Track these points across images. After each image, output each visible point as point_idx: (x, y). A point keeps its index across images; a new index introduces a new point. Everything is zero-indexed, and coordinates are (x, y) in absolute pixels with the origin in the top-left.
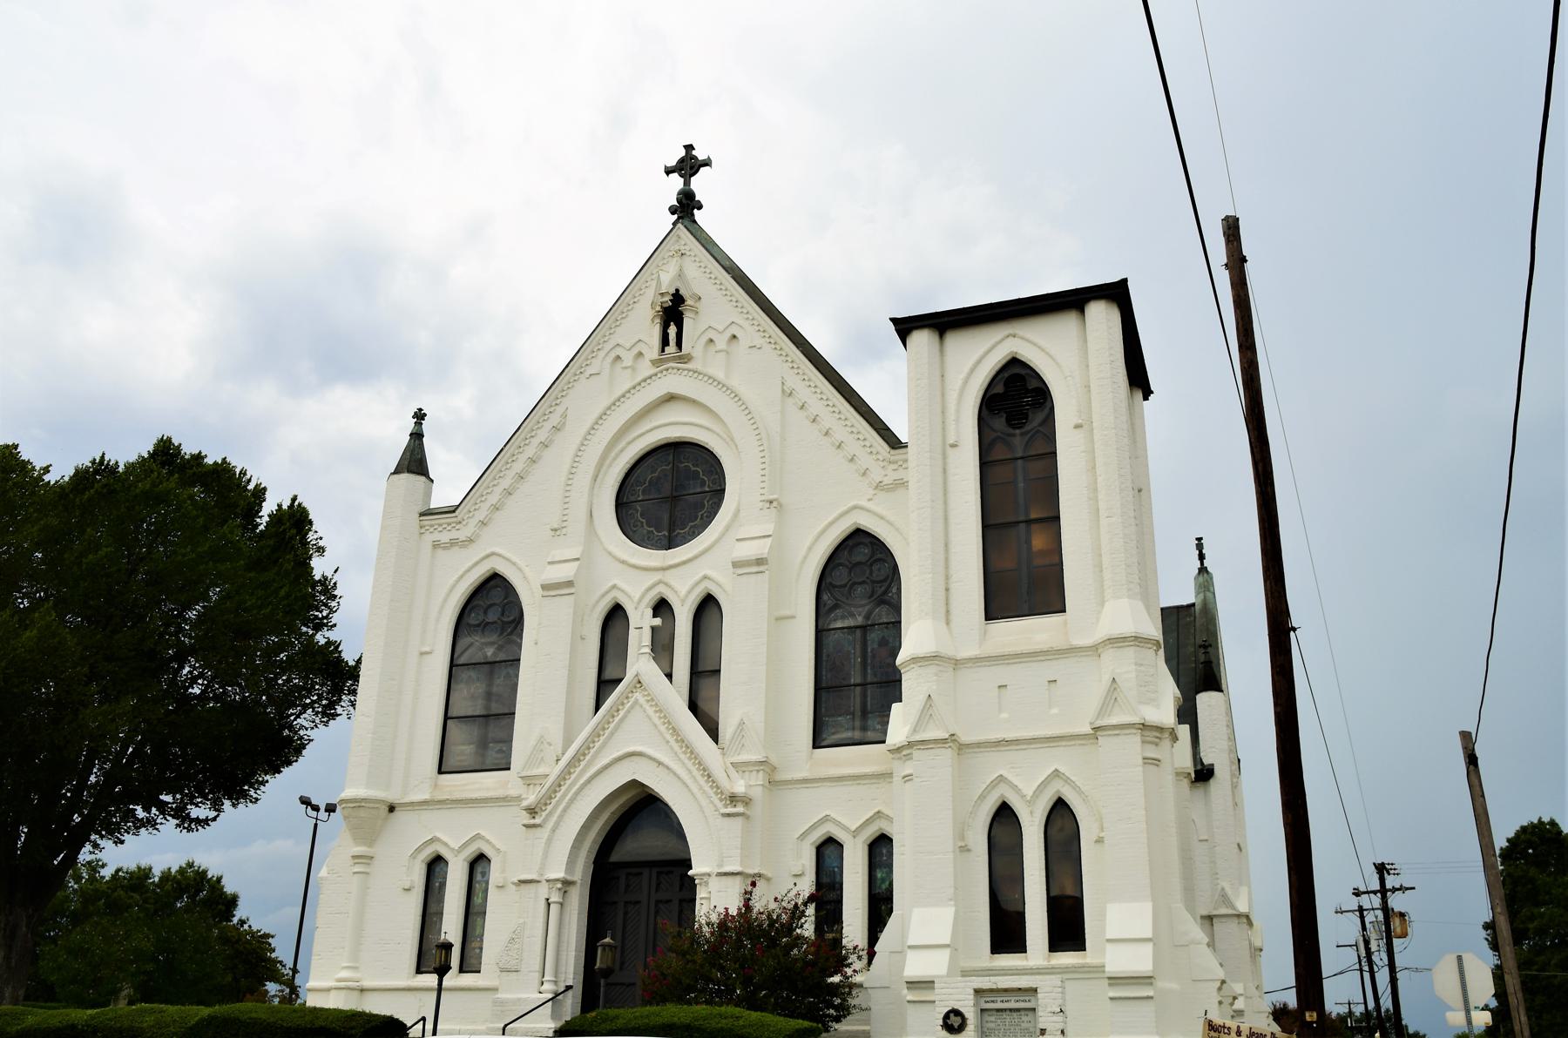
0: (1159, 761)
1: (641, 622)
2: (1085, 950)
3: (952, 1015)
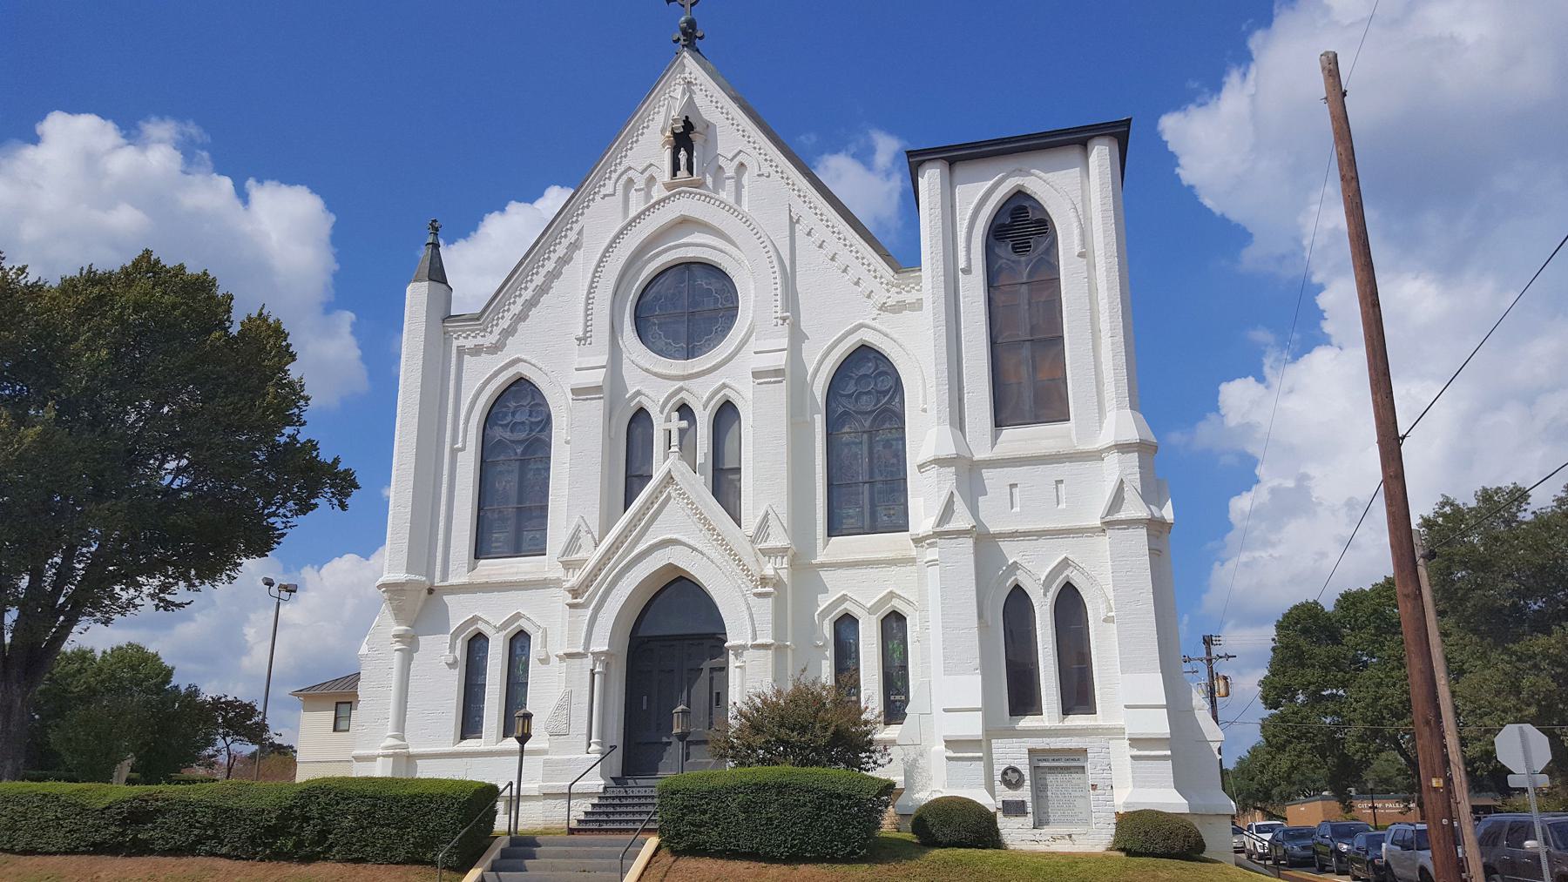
0: (1160, 552)
1: (663, 424)
2: (1095, 713)
3: (1009, 772)
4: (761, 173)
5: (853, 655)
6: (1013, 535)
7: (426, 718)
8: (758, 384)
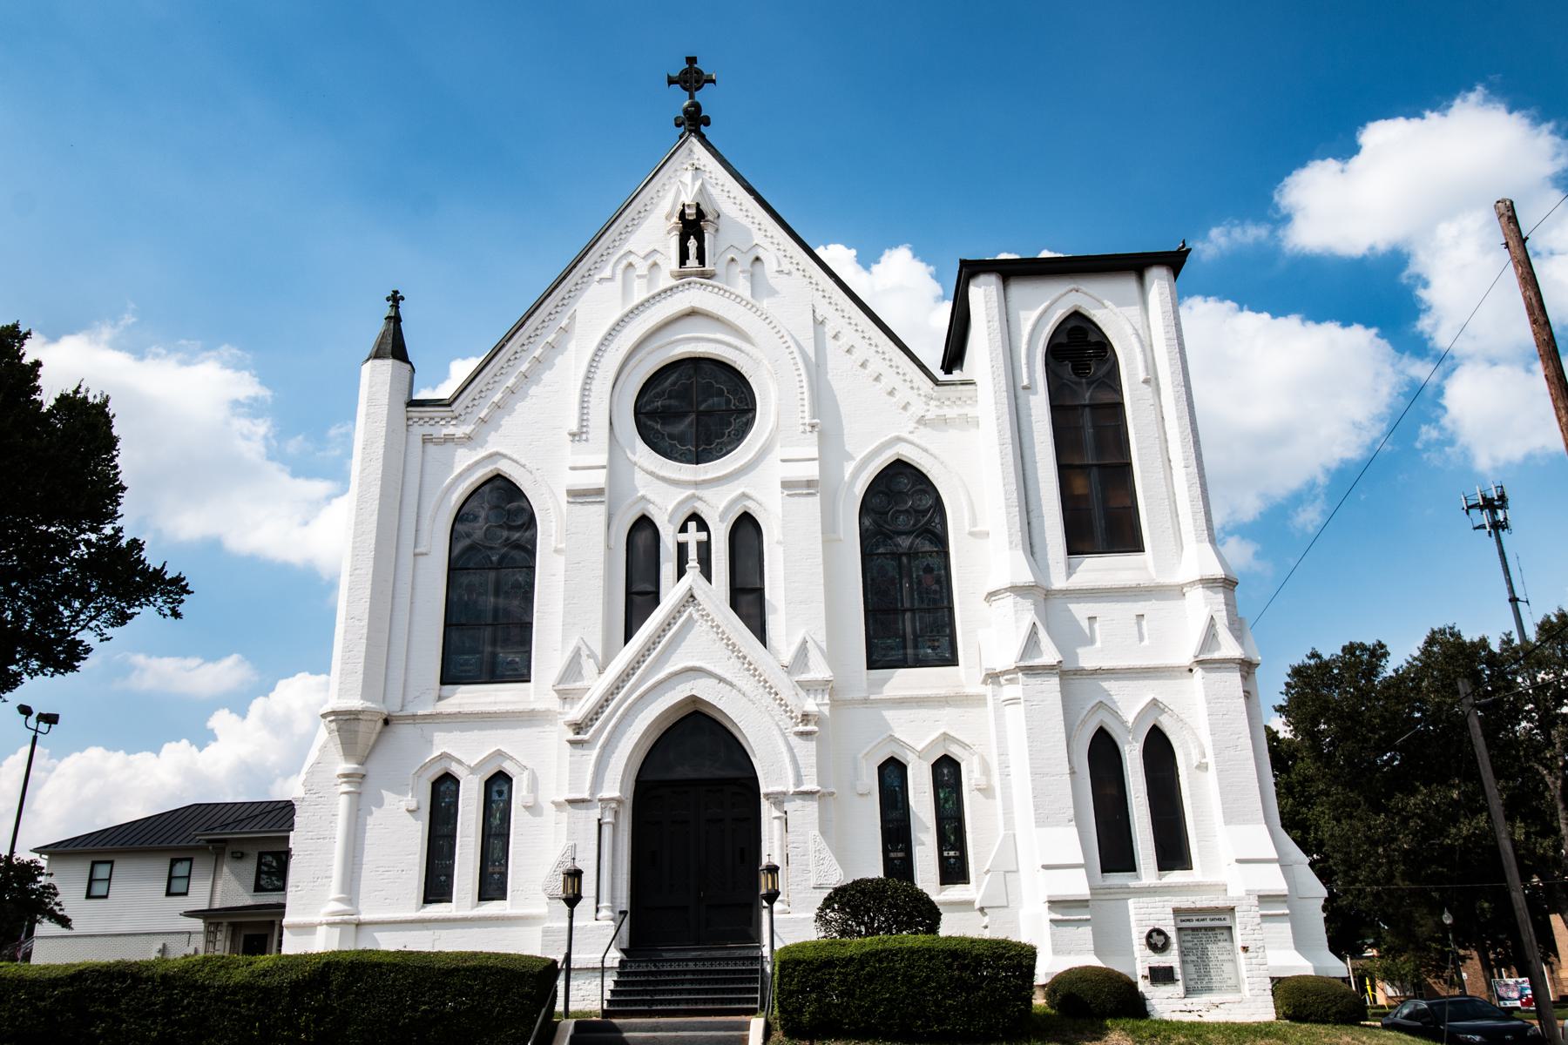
3: (1154, 934)
4: (780, 269)
5: (900, 805)
7: (382, 877)
8: (788, 495)
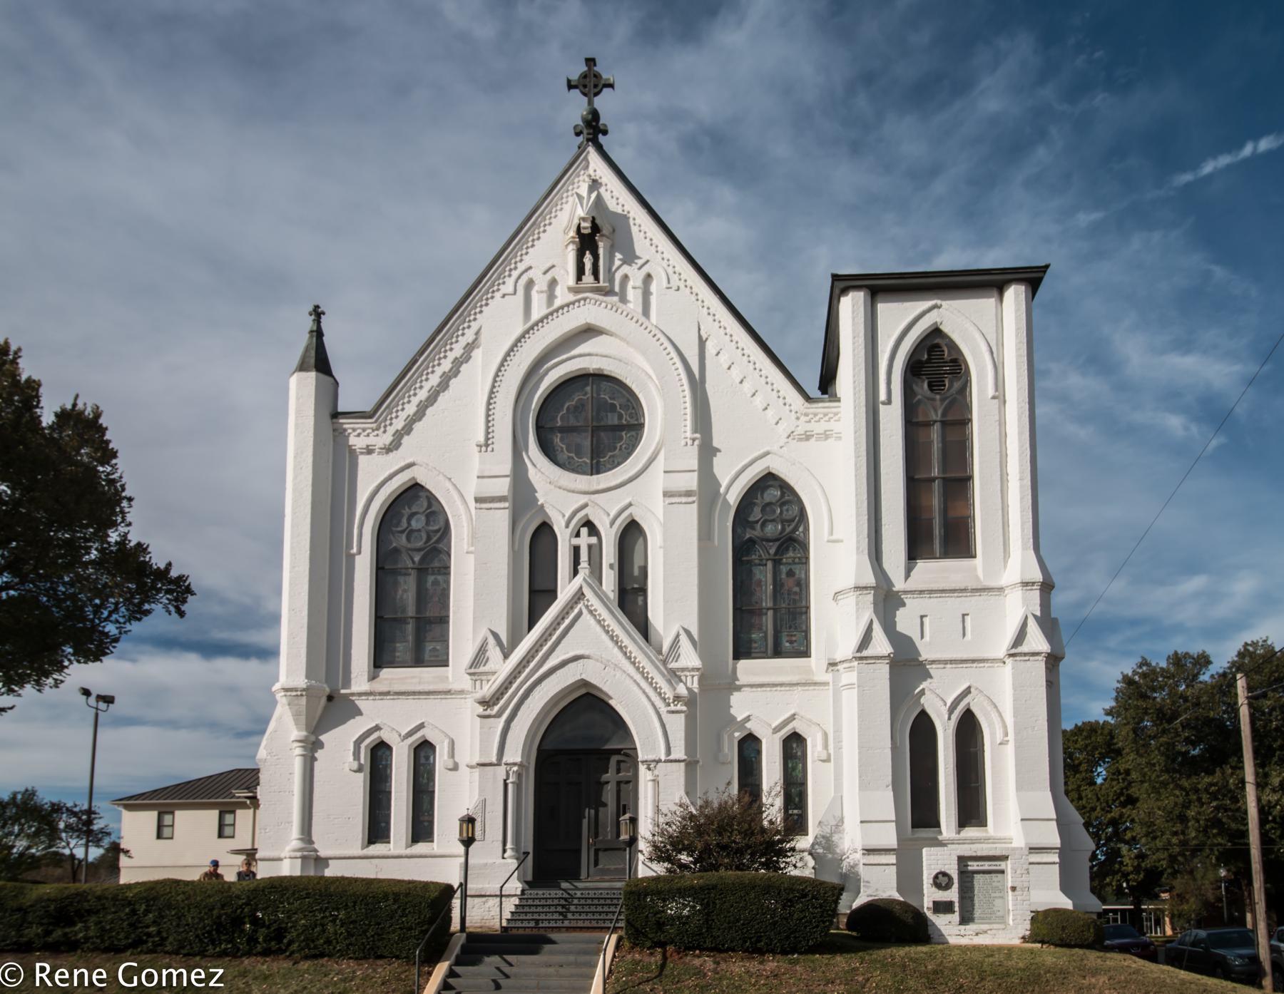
3: (940, 876)
6: (933, 662)
